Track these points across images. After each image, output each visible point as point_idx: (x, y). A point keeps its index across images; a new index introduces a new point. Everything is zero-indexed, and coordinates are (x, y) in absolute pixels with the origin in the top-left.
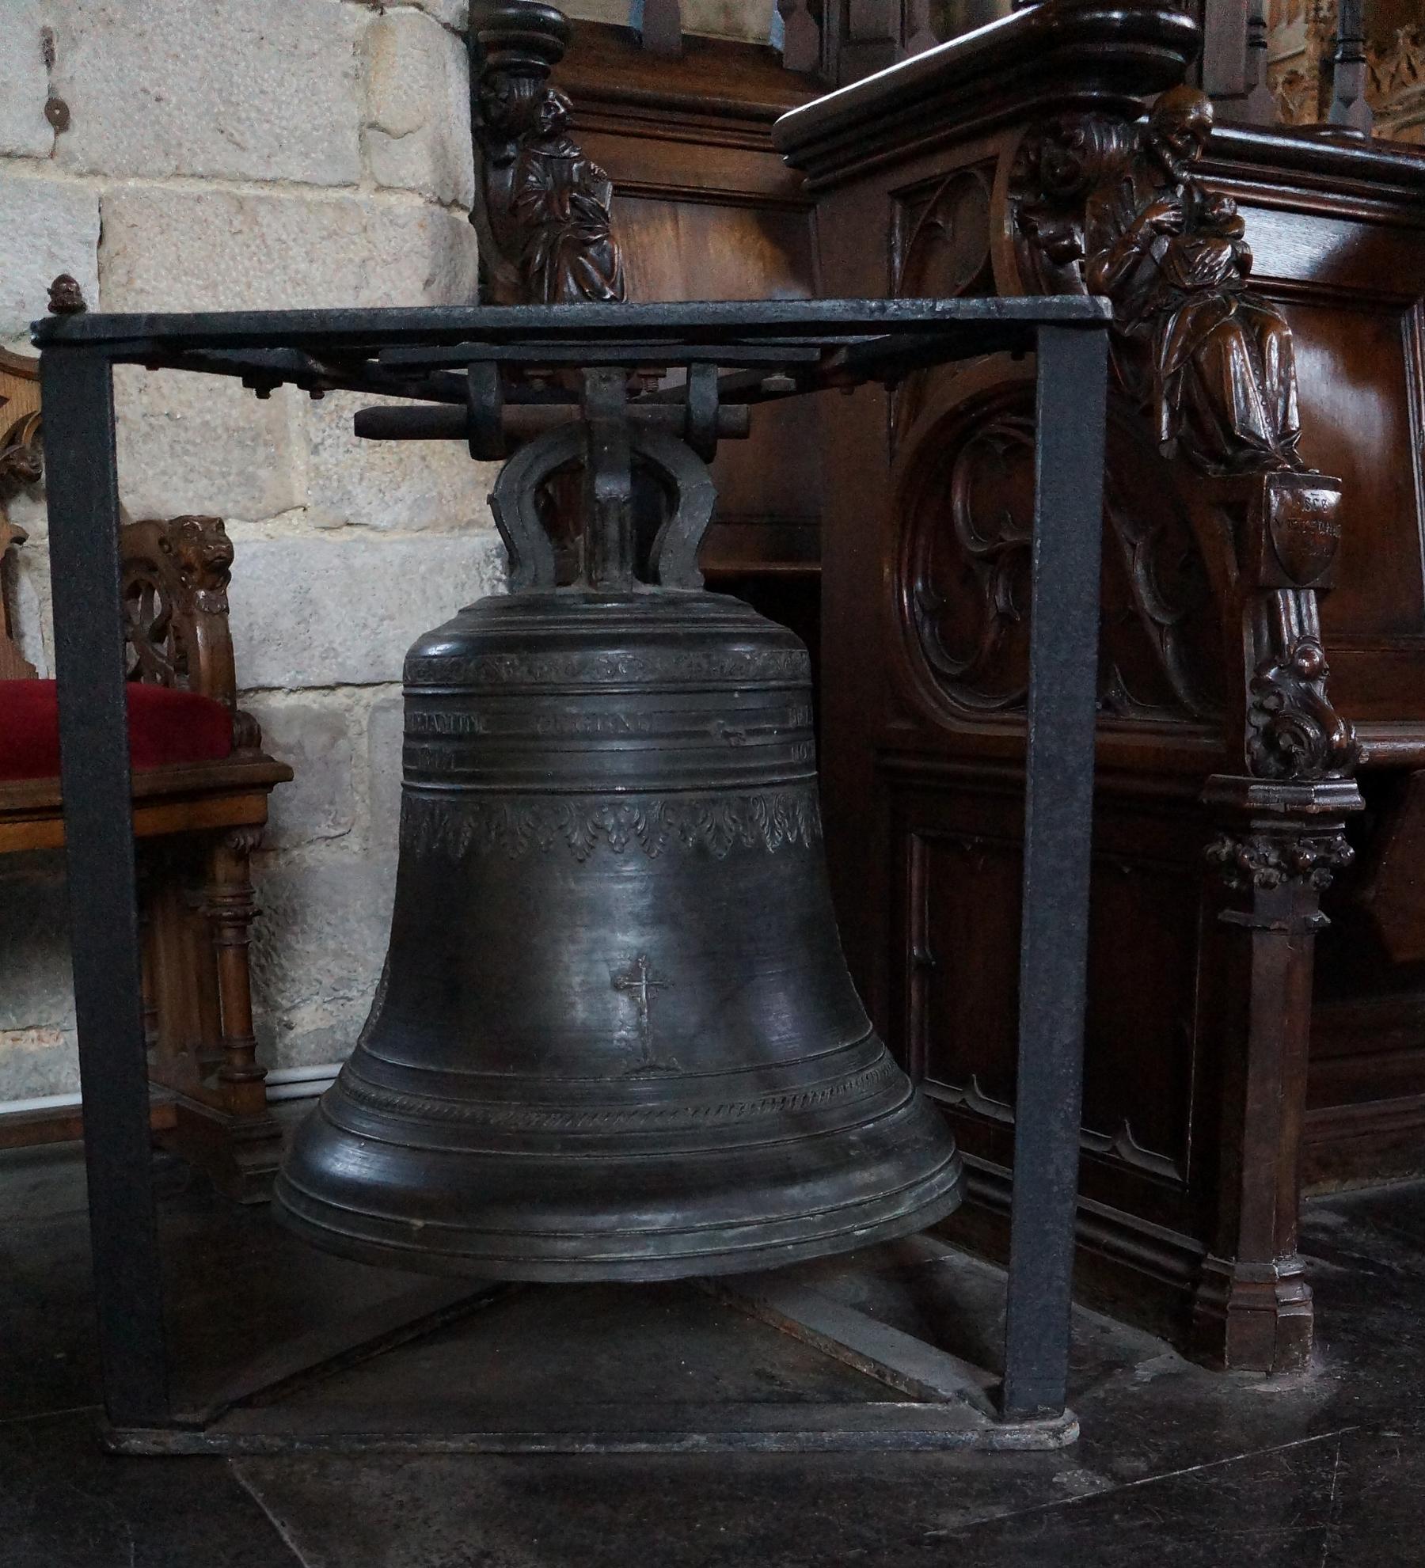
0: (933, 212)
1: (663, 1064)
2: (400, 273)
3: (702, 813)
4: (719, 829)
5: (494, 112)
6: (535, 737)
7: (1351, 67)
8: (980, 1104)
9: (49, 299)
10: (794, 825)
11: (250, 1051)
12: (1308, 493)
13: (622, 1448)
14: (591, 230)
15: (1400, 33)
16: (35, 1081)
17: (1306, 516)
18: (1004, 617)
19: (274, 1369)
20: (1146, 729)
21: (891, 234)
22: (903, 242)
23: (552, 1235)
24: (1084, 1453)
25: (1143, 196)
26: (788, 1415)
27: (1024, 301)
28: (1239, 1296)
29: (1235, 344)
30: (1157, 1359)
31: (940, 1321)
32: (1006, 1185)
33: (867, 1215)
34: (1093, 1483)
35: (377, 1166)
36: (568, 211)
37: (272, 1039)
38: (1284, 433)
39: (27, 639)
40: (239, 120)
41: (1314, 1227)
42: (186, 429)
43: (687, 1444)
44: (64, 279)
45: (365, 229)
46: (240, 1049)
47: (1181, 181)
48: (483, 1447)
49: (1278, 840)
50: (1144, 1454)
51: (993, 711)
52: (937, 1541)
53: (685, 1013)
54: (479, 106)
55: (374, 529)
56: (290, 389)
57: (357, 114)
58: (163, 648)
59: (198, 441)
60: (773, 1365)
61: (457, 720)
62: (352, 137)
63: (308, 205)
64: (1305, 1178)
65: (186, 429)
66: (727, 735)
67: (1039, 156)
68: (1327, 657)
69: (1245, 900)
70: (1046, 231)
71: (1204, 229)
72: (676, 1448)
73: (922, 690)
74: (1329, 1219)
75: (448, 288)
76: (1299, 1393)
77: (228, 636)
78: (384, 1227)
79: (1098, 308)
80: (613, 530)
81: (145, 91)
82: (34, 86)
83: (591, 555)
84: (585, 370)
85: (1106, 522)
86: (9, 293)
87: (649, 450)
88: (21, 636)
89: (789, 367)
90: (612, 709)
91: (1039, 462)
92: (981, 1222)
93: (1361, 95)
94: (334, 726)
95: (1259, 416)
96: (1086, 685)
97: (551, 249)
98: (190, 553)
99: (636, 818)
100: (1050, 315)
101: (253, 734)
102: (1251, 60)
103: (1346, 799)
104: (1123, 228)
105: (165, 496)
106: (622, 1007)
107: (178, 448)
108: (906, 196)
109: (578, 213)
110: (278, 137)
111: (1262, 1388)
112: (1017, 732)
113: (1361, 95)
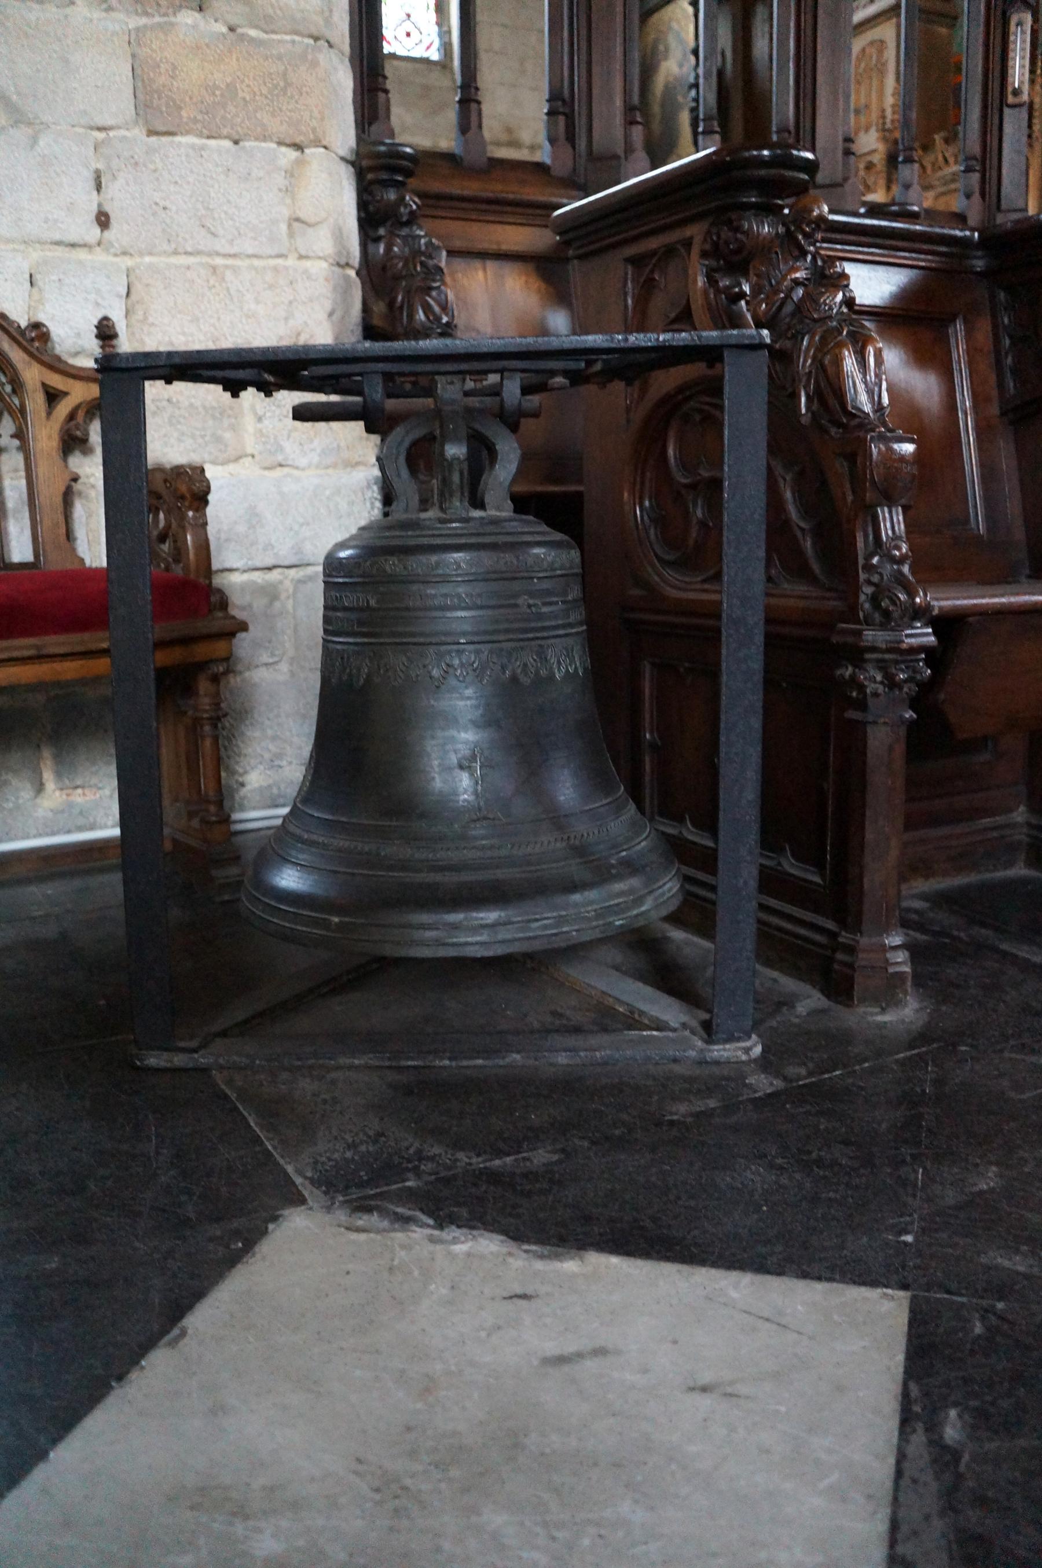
0: (652, 271)
1: (491, 816)
2: (313, 309)
4: (525, 665)
5: (371, 208)
6: (407, 609)
7: (908, 165)
8: (691, 834)
9: (95, 330)
10: (572, 661)
11: (220, 804)
12: (896, 446)
13: (465, 1063)
14: (434, 281)
16: (81, 821)
17: (895, 461)
18: (703, 524)
20: (797, 595)
21: (625, 285)
23: (423, 927)
24: (765, 1064)
25: (786, 262)
26: (571, 1041)
27: (714, 333)
28: (863, 958)
29: (847, 353)
30: (810, 1000)
31: (668, 976)
32: (713, 889)
33: (623, 911)
34: (771, 1084)
36: (419, 269)
37: (232, 792)
38: (879, 408)
39: (79, 542)
40: (214, 219)
41: (909, 910)
43: (507, 1060)
44: (106, 319)
45: (291, 283)
46: (215, 802)
47: (810, 252)
49: (882, 666)
50: (805, 1064)
52: (672, 1123)
54: (362, 205)
55: (297, 468)
56: (251, 391)
57: (286, 213)
58: (165, 547)
59: (187, 415)
61: (358, 598)
62: (284, 227)
63: (256, 269)
64: (903, 878)
65: (179, 408)
66: (530, 606)
67: (719, 237)
69: (862, 705)
70: (725, 282)
71: (825, 281)
72: (501, 1063)
73: (650, 570)
74: (918, 904)
75: (343, 317)
76: (903, 1021)
78: (315, 923)
79: (760, 335)
80: (456, 478)
81: (156, 204)
82: (90, 203)
83: (442, 494)
84: (436, 377)
86: (71, 328)
87: (477, 426)
88: (75, 539)
89: (566, 373)
90: (455, 590)
91: (726, 433)
92: (697, 912)
94: (271, 593)
95: (863, 398)
96: (758, 573)
97: (408, 292)
98: (183, 488)
99: (473, 659)
100: (733, 342)
102: (846, 164)
103: (925, 639)
104: (773, 282)
105: (166, 450)
106: (465, 781)
107: (174, 421)
109: (425, 270)
110: (237, 229)
111: (879, 1018)
113: (916, 180)
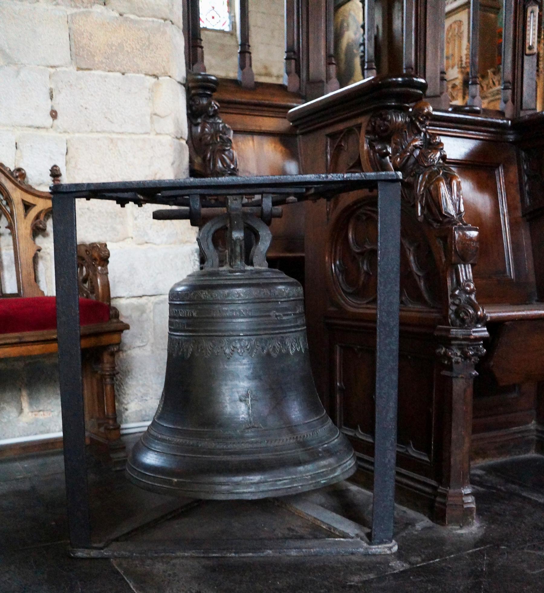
0: (340, 141)
3: (269, 342)
4: (274, 347)
5: (194, 108)
6: (213, 318)
7: (474, 86)
10: (299, 345)
11: (115, 419)
13: (243, 555)
14: (227, 146)
15: (489, 71)
16: (42, 429)
17: (467, 240)
18: (367, 273)
19: (125, 529)
20: (416, 310)
21: (326, 148)
22: (331, 151)
23: (221, 484)
24: (399, 555)
25: (410, 136)
26: (298, 543)
27: (373, 174)
28: (450, 500)
30: (423, 522)
31: (349, 509)
32: (372, 464)
33: (325, 476)
34: (403, 566)
35: (161, 461)
36: (219, 140)
37: (121, 413)
38: (459, 213)
40: (112, 114)
41: (474, 475)
42: (94, 213)
45: (152, 147)
46: (112, 418)
48: (197, 555)
49: (461, 347)
50: (420, 556)
51: (364, 304)
52: (351, 586)
53: (264, 409)
55: (155, 244)
56: (131, 204)
58: (86, 285)
60: (293, 526)
62: (148, 118)
64: (471, 459)
65: (94, 213)
66: (276, 316)
67: (375, 123)
68: (475, 286)
69: (450, 368)
71: (430, 147)
72: (262, 555)
74: (479, 472)
75: (179, 165)
76: (471, 533)
77: (108, 282)
80: (238, 249)
81: (82, 106)
82: (47, 106)
83: (231, 258)
84: (228, 197)
85: (402, 244)
87: (249, 222)
88: (39, 281)
89: (295, 195)
90: (238, 308)
91: (379, 225)
92: (363, 476)
93: (478, 94)
94: (142, 310)
96: (396, 299)
97: (213, 153)
98: (96, 255)
99: (247, 344)
100: (383, 178)
101: (117, 315)
102: (441, 85)
104: (404, 147)
108: (333, 136)
109: (222, 141)
111: (459, 532)
112: (373, 311)
113: (478, 94)
